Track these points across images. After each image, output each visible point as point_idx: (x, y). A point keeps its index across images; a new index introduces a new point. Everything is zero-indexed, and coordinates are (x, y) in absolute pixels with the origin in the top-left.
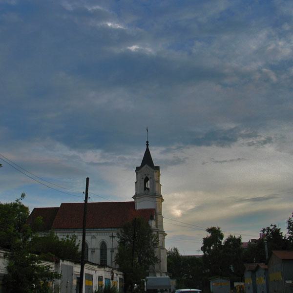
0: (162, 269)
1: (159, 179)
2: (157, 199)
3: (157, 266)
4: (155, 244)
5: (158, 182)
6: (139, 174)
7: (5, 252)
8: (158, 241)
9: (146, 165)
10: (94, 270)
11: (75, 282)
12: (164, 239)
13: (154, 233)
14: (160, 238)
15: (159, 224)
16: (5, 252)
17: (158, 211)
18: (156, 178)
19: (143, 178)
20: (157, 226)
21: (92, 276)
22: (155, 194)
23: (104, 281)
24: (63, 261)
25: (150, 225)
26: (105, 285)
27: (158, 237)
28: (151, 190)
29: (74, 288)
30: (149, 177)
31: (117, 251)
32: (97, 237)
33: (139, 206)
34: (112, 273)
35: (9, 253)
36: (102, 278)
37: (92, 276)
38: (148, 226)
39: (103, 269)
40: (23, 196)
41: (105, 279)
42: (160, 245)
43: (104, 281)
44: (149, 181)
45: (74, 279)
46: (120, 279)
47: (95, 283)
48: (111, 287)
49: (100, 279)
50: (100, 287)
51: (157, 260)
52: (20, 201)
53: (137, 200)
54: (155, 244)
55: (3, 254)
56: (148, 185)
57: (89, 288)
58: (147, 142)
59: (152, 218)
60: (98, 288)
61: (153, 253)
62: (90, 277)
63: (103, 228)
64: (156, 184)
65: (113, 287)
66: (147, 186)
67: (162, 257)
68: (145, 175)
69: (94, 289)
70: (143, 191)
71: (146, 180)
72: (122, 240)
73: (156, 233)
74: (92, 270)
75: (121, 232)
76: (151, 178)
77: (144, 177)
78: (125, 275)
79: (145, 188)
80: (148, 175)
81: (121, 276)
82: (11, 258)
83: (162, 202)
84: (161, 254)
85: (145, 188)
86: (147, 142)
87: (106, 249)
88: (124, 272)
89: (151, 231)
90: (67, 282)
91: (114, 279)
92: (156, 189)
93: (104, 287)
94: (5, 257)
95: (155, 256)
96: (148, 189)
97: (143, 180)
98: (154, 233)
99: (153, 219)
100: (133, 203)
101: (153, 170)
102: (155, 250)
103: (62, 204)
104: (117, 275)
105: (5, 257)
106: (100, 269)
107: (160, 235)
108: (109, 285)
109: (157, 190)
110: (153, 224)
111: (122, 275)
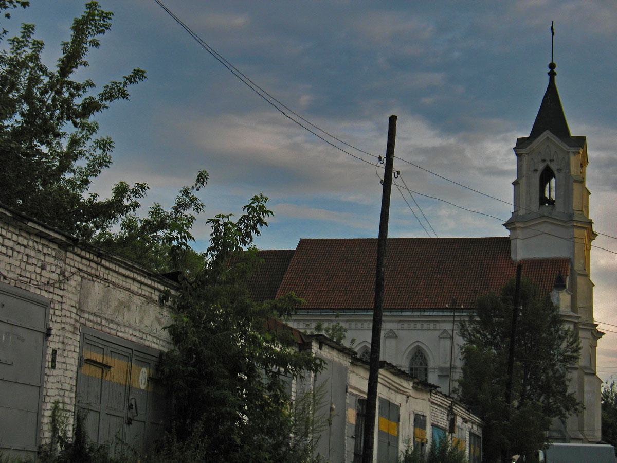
0: (586, 432)
1: (583, 173)
2: (577, 232)
3: (572, 420)
4: (571, 358)
5: (582, 181)
6: (525, 159)
7: (162, 288)
8: (577, 350)
9: (547, 134)
10: (403, 393)
11: (351, 416)
12: (594, 346)
13: (566, 326)
14: (584, 343)
15: (580, 304)
16: (162, 288)
17: (578, 266)
18: (574, 170)
19: (536, 171)
20: (574, 307)
21: (397, 408)
22: (571, 217)
23: (429, 429)
24: (320, 348)
25: (555, 302)
26: (434, 442)
27: (576, 339)
28: (560, 207)
29: (350, 431)
30: (554, 167)
31: (458, 375)
32: (401, 334)
33: (520, 253)
34: (451, 412)
35: (173, 292)
36: (425, 421)
37: (397, 408)
38: (551, 307)
39: (426, 396)
40: (202, 179)
41: (433, 425)
42: (582, 362)
43: (429, 429)
44: (553, 180)
45: (350, 406)
46: (472, 435)
47: (406, 430)
48: (450, 449)
49: (419, 421)
50: (420, 444)
51: (572, 404)
52: (194, 193)
53: (519, 232)
54: (570, 359)
55: (157, 293)
56: (552, 186)
57: (390, 441)
58: (552, 66)
59: (560, 284)
60: (412, 444)
61: (561, 381)
62: (392, 411)
63: (419, 310)
64: (576, 187)
65: (451, 452)
66: (547, 195)
67: (587, 397)
68: (544, 161)
69: (402, 447)
70: (535, 206)
71: (547, 175)
72: (472, 342)
73: (572, 327)
74: (398, 391)
75: (471, 321)
76: (559, 170)
77: (541, 167)
78: (486, 428)
79: (543, 200)
80: (551, 161)
81: (475, 428)
82: (179, 309)
83: (591, 240)
84: (586, 388)
85: (543, 200)
86: (552, 66)
87: (426, 370)
88: (483, 419)
89: (557, 320)
90: (331, 409)
91: (457, 430)
92: (574, 204)
93: (428, 447)
94: (162, 301)
95: (569, 391)
96: (551, 202)
97: (538, 175)
98: (566, 326)
99: (564, 286)
100: (505, 241)
101: (565, 147)
102: (569, 376)
103: (303, 242)
104: (465, 421)
105: (162, 301)
106: (419, 395)
107: (582, 334)
108: (444, 442)
109: (576, 203)
110: (563, 300)
111: (479, 425)
